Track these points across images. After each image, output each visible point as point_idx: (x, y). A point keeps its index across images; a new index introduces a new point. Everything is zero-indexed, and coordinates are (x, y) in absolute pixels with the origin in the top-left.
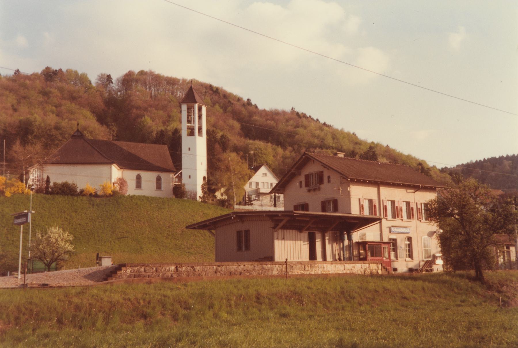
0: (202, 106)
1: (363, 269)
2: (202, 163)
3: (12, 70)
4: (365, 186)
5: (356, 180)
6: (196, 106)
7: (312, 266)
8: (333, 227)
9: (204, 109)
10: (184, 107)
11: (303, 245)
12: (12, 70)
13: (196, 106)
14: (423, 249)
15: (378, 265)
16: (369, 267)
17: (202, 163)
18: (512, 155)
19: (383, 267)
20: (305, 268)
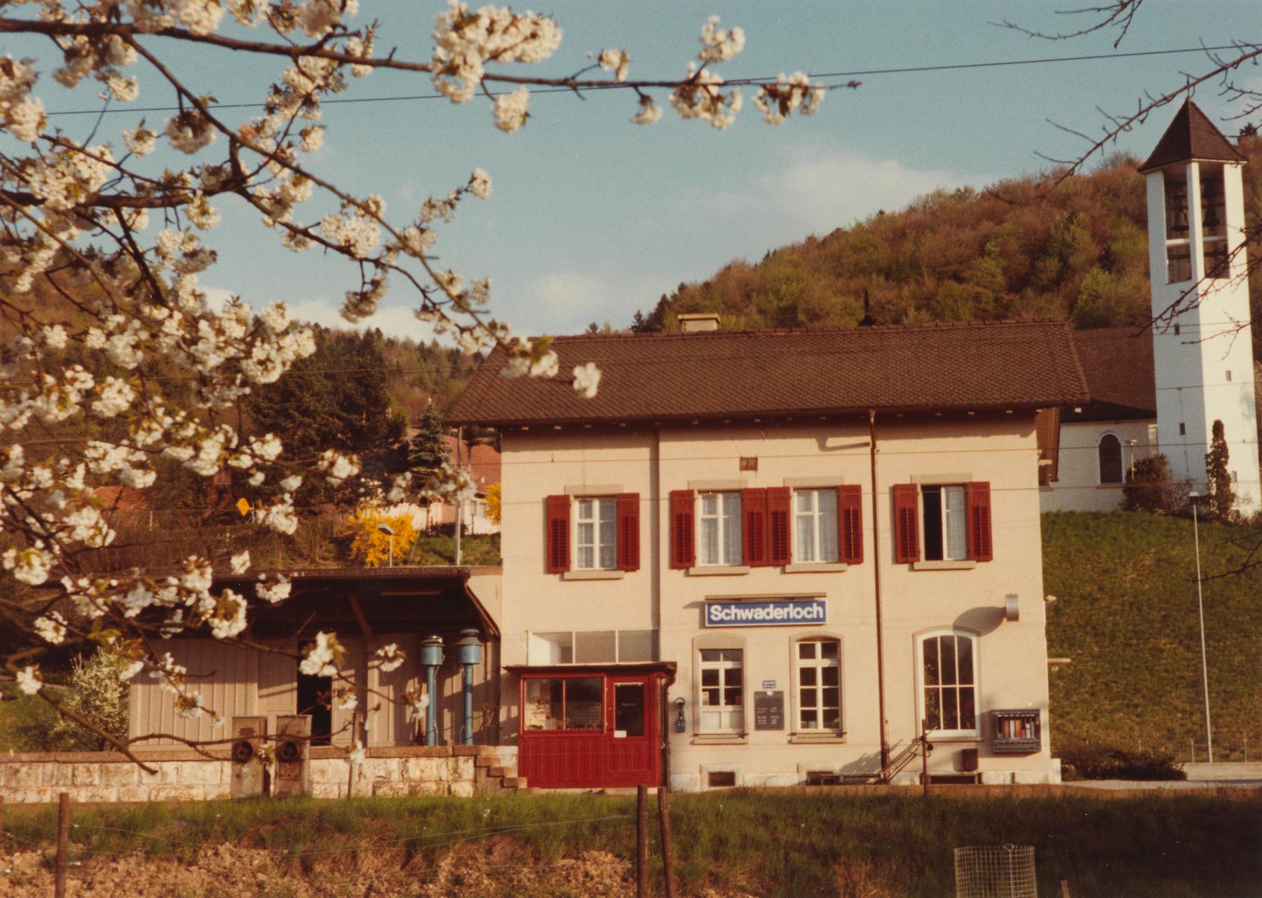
0: (1222, 165)
1: (372, 779)
2: (1182, 426)
3: (1091, 140)
4: (784, 437)
5: (1078, 410)
6: (1194, 170)
7: (107, 768)
8: (309, 620)
9: (1233, 176)
10: (1156, 187)
11: (260, 697)
12: (1091, 140)
13: (1194, 170)
14: (922, 686)
15: (457, 762)
16: (404, 770)
17: (1182, 426)
18: (853, 225)
19: (483, 772)
20: (74, 775)
